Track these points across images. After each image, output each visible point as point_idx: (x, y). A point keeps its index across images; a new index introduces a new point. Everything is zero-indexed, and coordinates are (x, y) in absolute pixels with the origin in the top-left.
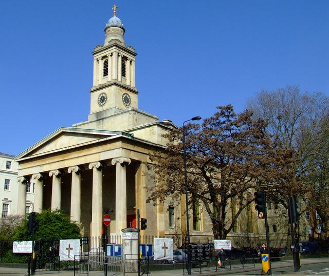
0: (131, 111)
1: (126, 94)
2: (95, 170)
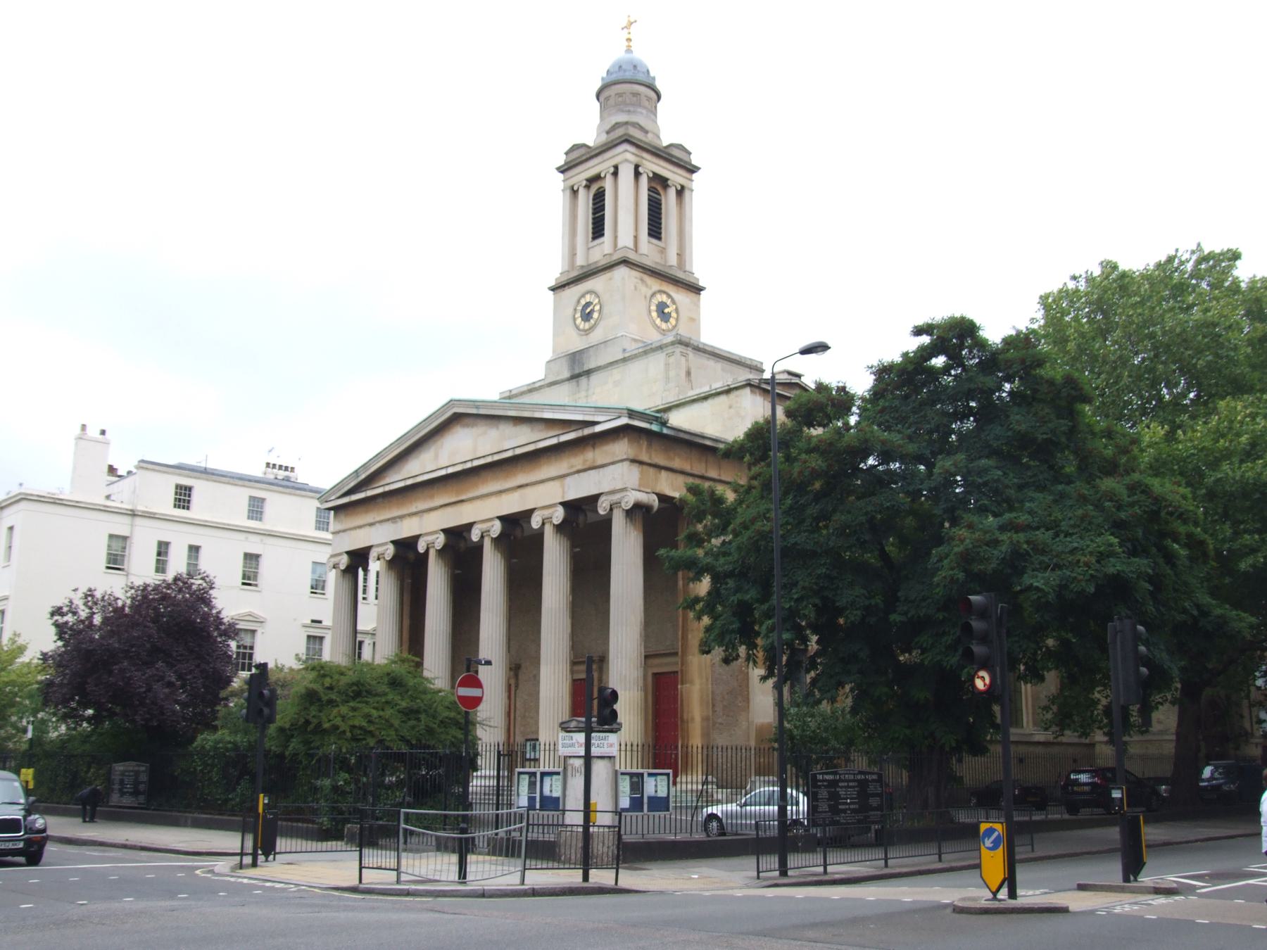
0: (673, 343)
2: (549, 533)
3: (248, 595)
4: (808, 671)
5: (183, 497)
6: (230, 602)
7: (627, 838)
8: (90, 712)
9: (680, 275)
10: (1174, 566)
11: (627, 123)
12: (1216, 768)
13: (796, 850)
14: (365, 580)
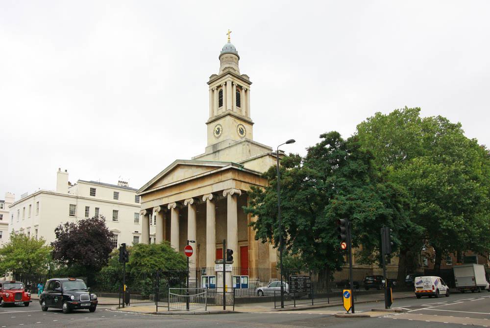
0: (245, 141)
1: (241, 124)
3: (114, 223)
4: (287, 245)
5: (93, 192)
6: (110, 226)
7: (235, 297)
8: (67, 261)
9: (247, 119)
10: (399, 211)
11: (229, 67)
12: (410, 276)
13: (286, 300)
14: (151, 218)
